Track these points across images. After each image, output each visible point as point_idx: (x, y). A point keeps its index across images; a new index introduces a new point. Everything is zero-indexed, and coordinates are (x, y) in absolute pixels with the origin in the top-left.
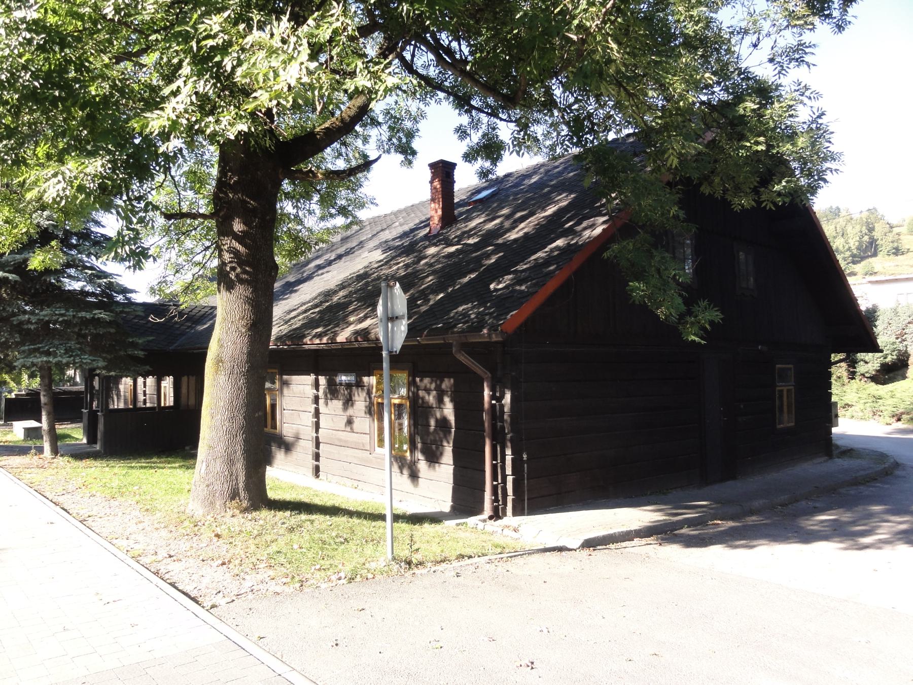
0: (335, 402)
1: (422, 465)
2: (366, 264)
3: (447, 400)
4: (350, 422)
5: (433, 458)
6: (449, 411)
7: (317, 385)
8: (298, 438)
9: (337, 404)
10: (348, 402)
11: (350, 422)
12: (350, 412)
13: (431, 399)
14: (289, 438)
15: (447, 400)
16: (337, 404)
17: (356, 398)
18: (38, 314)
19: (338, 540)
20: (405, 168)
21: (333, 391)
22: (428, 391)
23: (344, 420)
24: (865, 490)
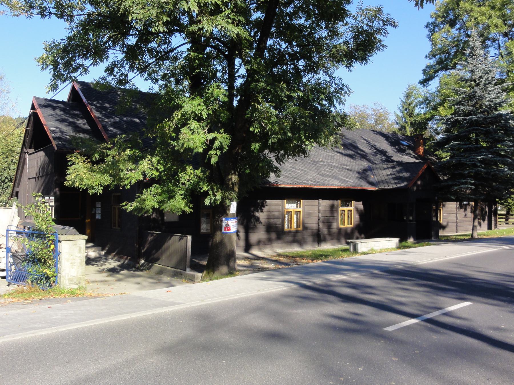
0: (462, 210)
1: (482, 222)
2: (388, 146)
3: (487, 207)
4: (466, 215)
5: (484, 220)
6: (487, 209)
7: (457, 205)
8: (448, 223)
9: (463, 210)
10: (465, 210)
11: (466, 215)
12: (466, 212)
13: (484, 207)
14: (444, 224)
15: (487, 207)
16: (463, 210)
17: (467, 208)
18: (455, 6)
19: (97, 379)
20: (425, 28)
21: (461, 207)
22: (483, 205)
23: (464, 214)
24: (317, 286)
